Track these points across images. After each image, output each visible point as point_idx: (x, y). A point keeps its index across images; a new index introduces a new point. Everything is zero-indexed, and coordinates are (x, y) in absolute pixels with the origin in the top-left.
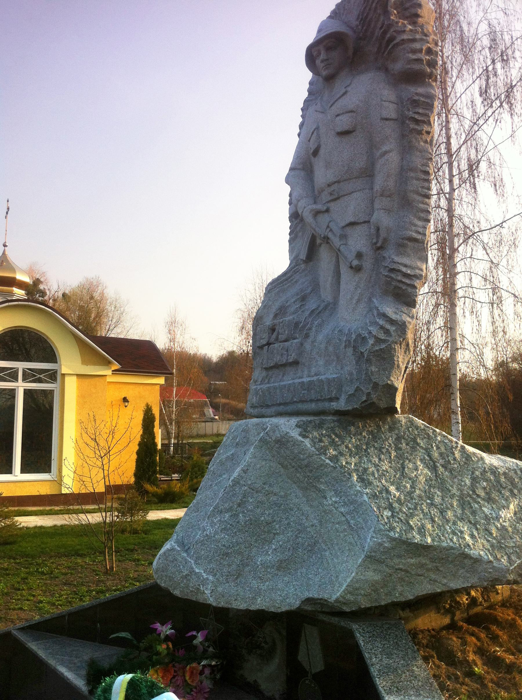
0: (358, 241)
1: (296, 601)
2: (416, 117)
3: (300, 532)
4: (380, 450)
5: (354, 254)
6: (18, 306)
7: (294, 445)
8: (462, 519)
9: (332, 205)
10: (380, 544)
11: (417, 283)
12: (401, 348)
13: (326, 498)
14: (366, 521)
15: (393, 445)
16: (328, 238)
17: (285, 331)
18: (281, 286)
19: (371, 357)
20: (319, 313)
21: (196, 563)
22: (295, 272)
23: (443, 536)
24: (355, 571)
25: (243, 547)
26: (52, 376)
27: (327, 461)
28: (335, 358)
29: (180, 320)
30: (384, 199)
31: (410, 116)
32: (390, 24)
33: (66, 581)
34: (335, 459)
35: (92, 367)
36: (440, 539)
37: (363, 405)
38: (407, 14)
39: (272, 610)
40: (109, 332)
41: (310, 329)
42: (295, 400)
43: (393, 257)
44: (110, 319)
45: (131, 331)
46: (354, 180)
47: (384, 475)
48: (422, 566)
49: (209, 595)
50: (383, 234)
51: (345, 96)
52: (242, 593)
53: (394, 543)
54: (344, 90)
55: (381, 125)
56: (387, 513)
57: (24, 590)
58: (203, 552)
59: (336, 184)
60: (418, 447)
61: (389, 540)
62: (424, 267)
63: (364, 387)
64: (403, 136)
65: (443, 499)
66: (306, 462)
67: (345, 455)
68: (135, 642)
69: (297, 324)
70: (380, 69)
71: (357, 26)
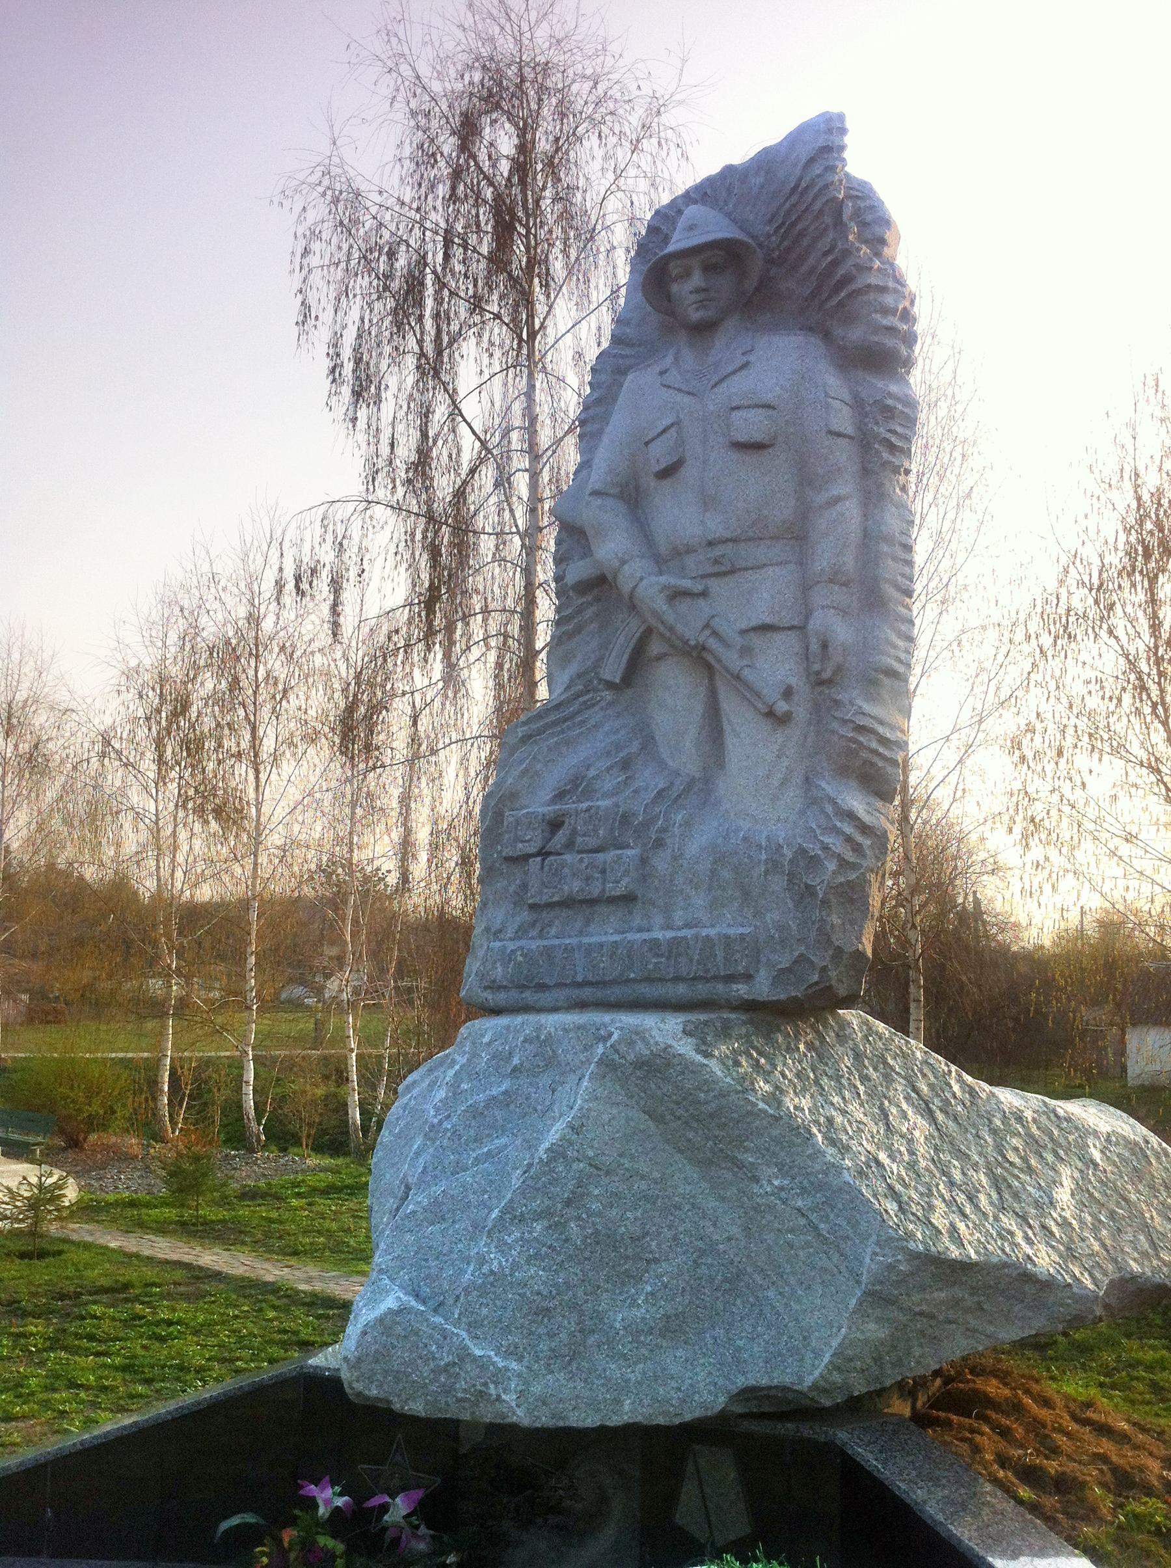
2: (893, 440)
3: (702, 1253)
7: (683, 1073)
9: (714, 585)
10: (891, 1267)
13: (757, 1181)
14: (855, 1225)
18: (563, 732)
25: (580, 1293)
27: (761, 1105)
28: (738, 894)
37: (810, 991)
39: (661, 1421)
42: (632, 975)
43: (859, 702)
46: (768, 542)
49: (513, 1404)
51: (744, 372)
53: (916, 1262)
55: (827, 443)
58: (485, 1311)
59: (730, 545)
70: (811, 329)
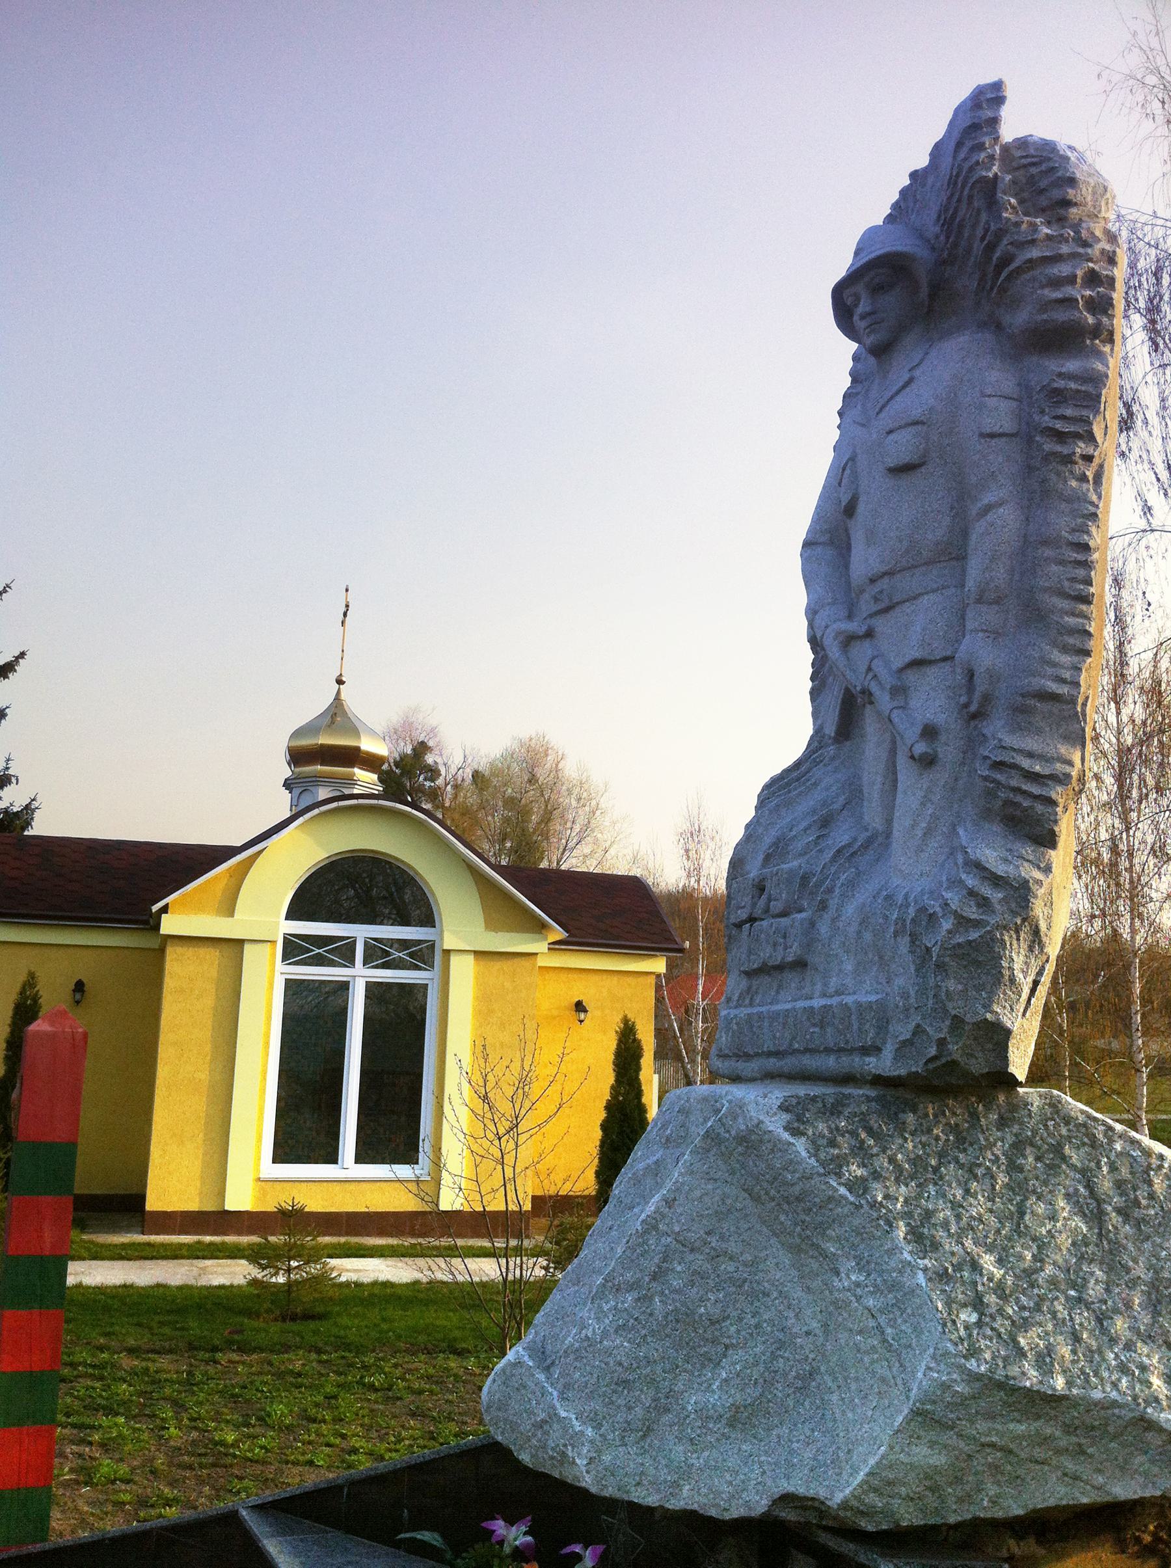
0: (931, 700)
1: (761, 1498)
2: (1057, 426)
3: (781, 1345)
4: (971, 1170)
5: (918, 730)
6: (362, 808)
8: (1150, 1336)
10: (946, 1387)
11: (1058, 793)
12: (1018, 940)
13: (838, 1274)
15: (1003, 1159)
16: (871, 694)
17: (780, 894)
19: (947, 959)
20: (852, 855)
21: (563, 1398)
22: (817, 763)
23: (1096, 1375)
24: (886, 1439)
25: (659, 1370)
26: (422, 955)
27: (842, 1190)
29: (710, 827)
30: (984, 608)
31: (1044, 425)
32: (1001, 229)
33: (417, 1408)
34: (859, 1186)
35: (508, 935)
36: (1087, 1380)
37: (931, 1066)
38: (1044, 202)
39: (713, 1513)
40: (567, 854)
41: (830, 890)
42: (797, 1046)
44: (569, 825)
45: (612, 852)
47: (972, 1229)
48: (1045, 1441)
49: (584, 1469)
50: (981, 686)
52: (652, 1471)
53: (977, 1385)
54: (906, 377)
56: (968, 1316)
57: (324, 1421)
59: (886, 580)
60: (1064, 1167)
61: (965, 1377)
62: (1076, 758)
63: (931, 1025)
64: (1030, 469)
65: (1108, 1290)
66: (796, 1190)
67: (886, 1178)
68: (449, 1556)
69: (805, 879)
71: (937, 237)
